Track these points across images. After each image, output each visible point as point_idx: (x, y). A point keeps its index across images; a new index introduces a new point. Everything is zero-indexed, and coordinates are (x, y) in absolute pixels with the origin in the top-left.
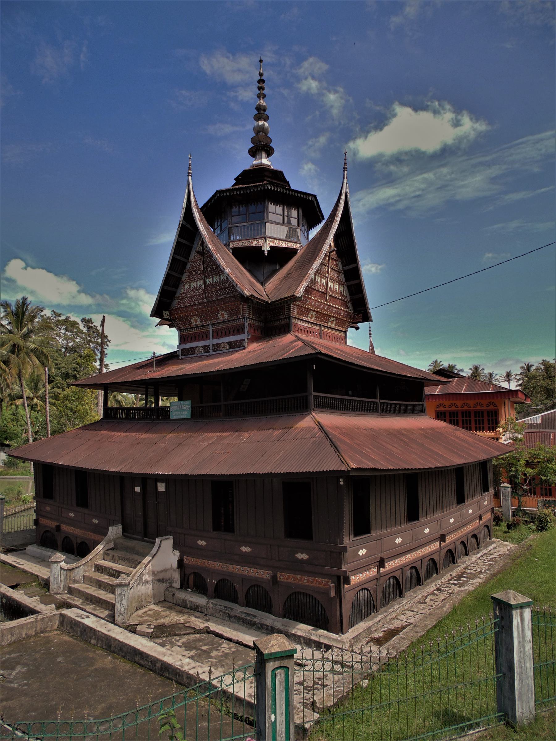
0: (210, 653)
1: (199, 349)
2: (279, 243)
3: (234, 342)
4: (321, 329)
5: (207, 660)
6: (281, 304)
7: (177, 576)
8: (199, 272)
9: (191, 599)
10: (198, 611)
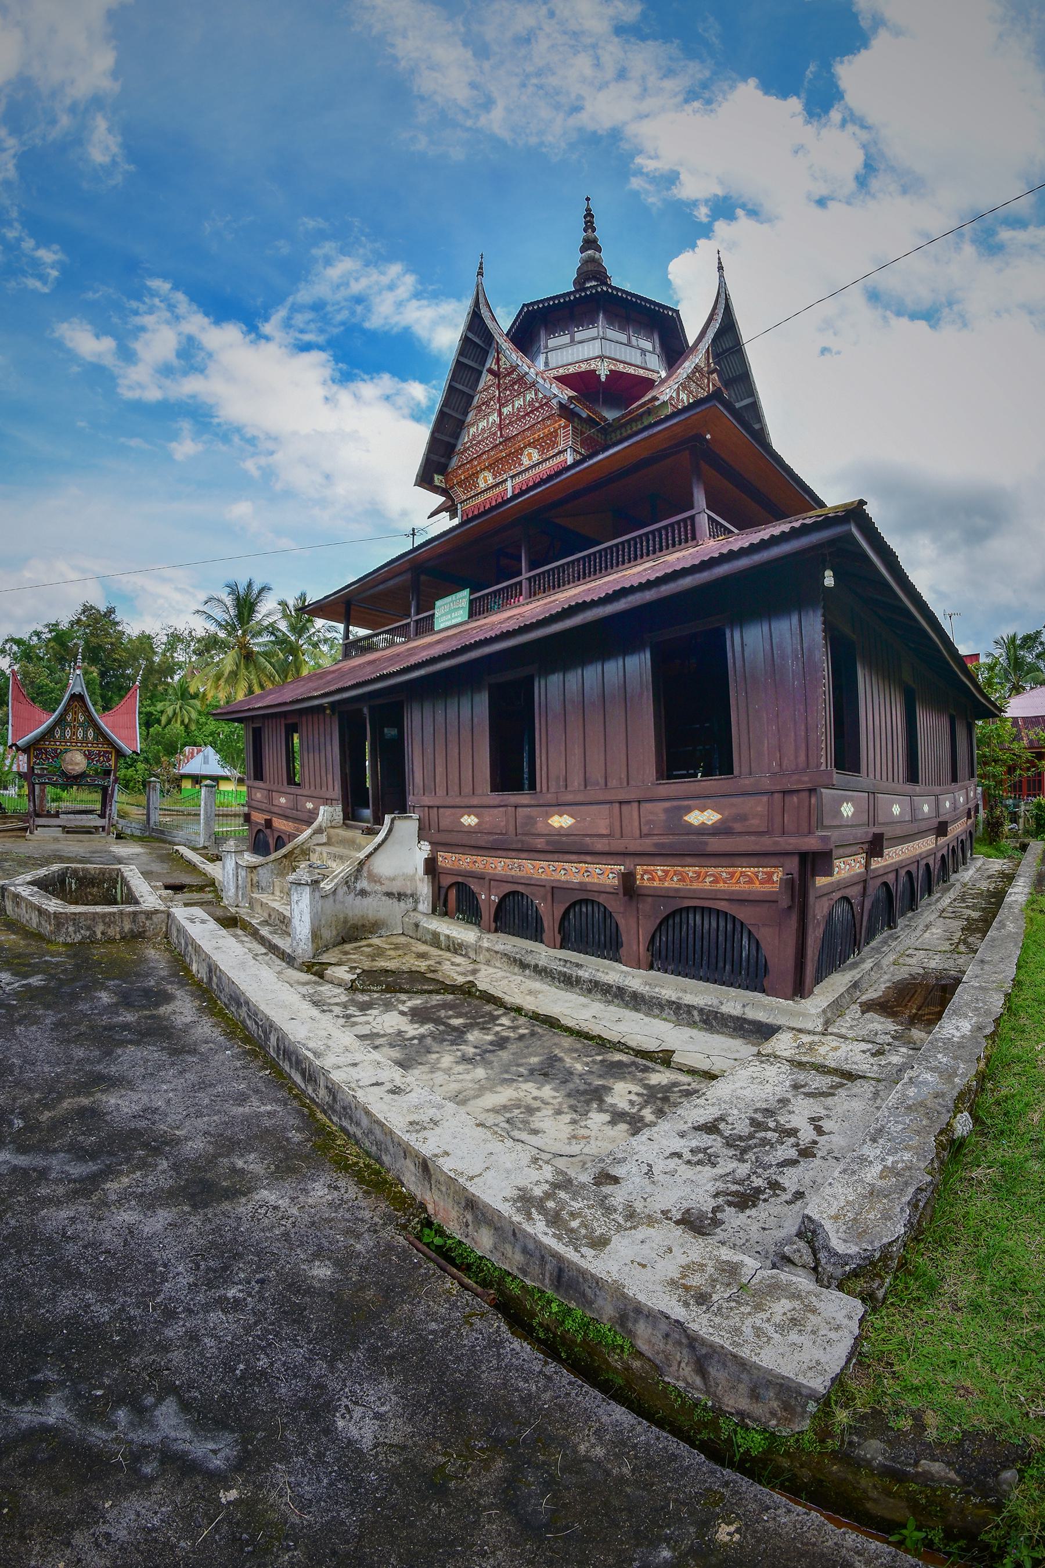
0: (464, 1033)
5: (455, 1047)
7: (425, 889)
9: (447, 932)
10: (461, 955)
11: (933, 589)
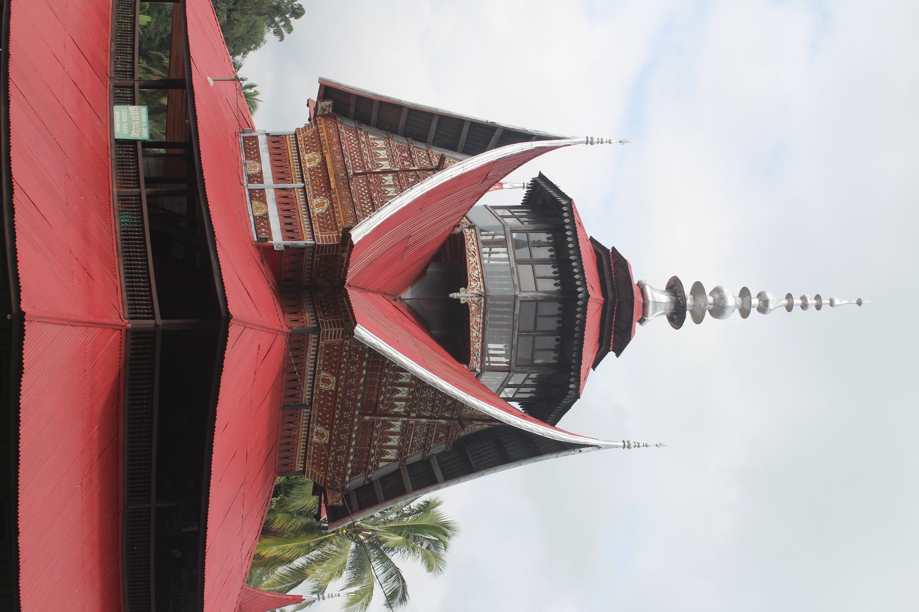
1: (255, 167)
2: (477, 323)
3: (269, 224)
4: (305, 406)
6: (345, 311)
8: (406, 163)
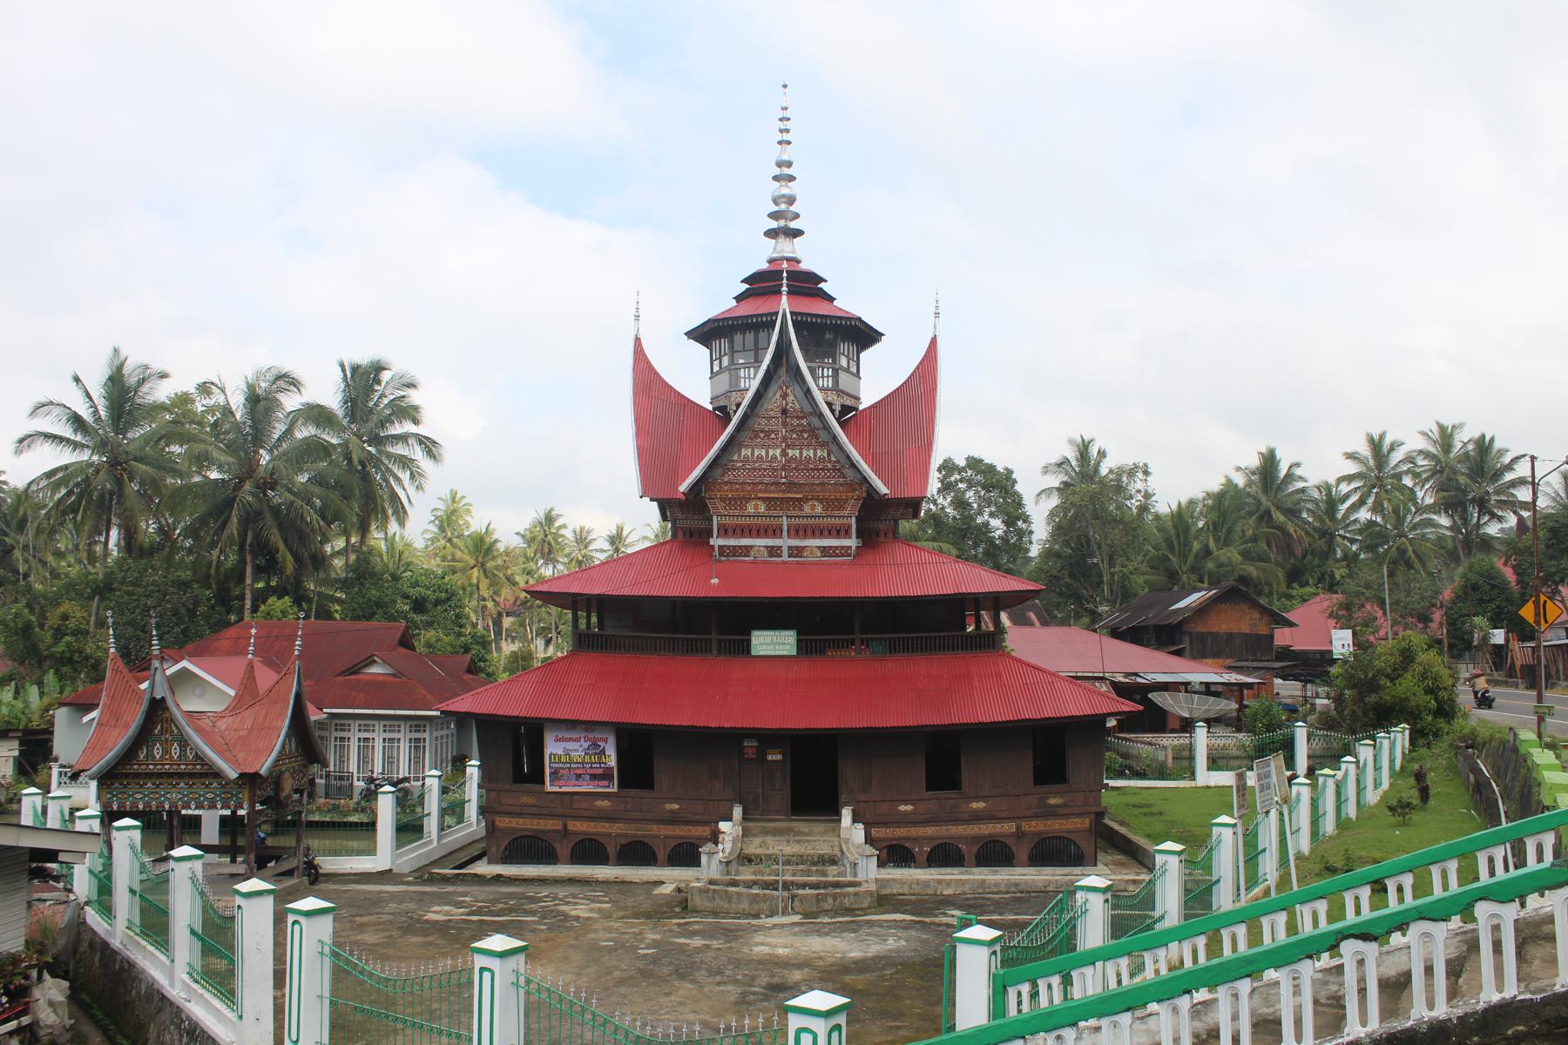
11: (281, 716)
